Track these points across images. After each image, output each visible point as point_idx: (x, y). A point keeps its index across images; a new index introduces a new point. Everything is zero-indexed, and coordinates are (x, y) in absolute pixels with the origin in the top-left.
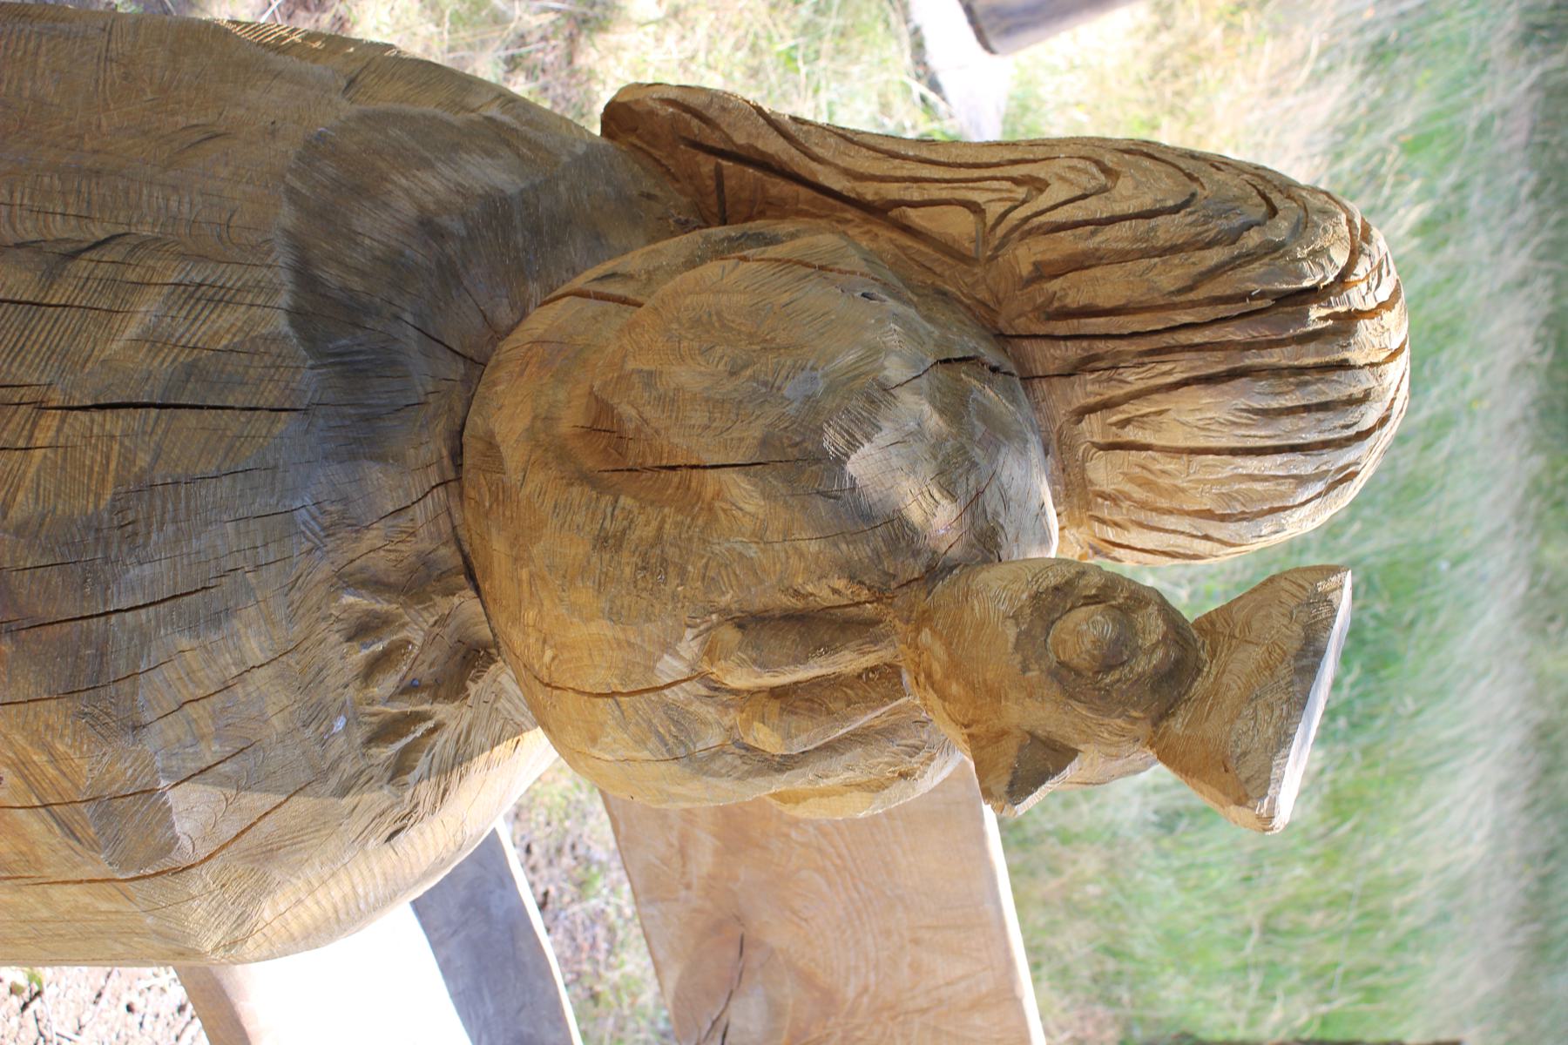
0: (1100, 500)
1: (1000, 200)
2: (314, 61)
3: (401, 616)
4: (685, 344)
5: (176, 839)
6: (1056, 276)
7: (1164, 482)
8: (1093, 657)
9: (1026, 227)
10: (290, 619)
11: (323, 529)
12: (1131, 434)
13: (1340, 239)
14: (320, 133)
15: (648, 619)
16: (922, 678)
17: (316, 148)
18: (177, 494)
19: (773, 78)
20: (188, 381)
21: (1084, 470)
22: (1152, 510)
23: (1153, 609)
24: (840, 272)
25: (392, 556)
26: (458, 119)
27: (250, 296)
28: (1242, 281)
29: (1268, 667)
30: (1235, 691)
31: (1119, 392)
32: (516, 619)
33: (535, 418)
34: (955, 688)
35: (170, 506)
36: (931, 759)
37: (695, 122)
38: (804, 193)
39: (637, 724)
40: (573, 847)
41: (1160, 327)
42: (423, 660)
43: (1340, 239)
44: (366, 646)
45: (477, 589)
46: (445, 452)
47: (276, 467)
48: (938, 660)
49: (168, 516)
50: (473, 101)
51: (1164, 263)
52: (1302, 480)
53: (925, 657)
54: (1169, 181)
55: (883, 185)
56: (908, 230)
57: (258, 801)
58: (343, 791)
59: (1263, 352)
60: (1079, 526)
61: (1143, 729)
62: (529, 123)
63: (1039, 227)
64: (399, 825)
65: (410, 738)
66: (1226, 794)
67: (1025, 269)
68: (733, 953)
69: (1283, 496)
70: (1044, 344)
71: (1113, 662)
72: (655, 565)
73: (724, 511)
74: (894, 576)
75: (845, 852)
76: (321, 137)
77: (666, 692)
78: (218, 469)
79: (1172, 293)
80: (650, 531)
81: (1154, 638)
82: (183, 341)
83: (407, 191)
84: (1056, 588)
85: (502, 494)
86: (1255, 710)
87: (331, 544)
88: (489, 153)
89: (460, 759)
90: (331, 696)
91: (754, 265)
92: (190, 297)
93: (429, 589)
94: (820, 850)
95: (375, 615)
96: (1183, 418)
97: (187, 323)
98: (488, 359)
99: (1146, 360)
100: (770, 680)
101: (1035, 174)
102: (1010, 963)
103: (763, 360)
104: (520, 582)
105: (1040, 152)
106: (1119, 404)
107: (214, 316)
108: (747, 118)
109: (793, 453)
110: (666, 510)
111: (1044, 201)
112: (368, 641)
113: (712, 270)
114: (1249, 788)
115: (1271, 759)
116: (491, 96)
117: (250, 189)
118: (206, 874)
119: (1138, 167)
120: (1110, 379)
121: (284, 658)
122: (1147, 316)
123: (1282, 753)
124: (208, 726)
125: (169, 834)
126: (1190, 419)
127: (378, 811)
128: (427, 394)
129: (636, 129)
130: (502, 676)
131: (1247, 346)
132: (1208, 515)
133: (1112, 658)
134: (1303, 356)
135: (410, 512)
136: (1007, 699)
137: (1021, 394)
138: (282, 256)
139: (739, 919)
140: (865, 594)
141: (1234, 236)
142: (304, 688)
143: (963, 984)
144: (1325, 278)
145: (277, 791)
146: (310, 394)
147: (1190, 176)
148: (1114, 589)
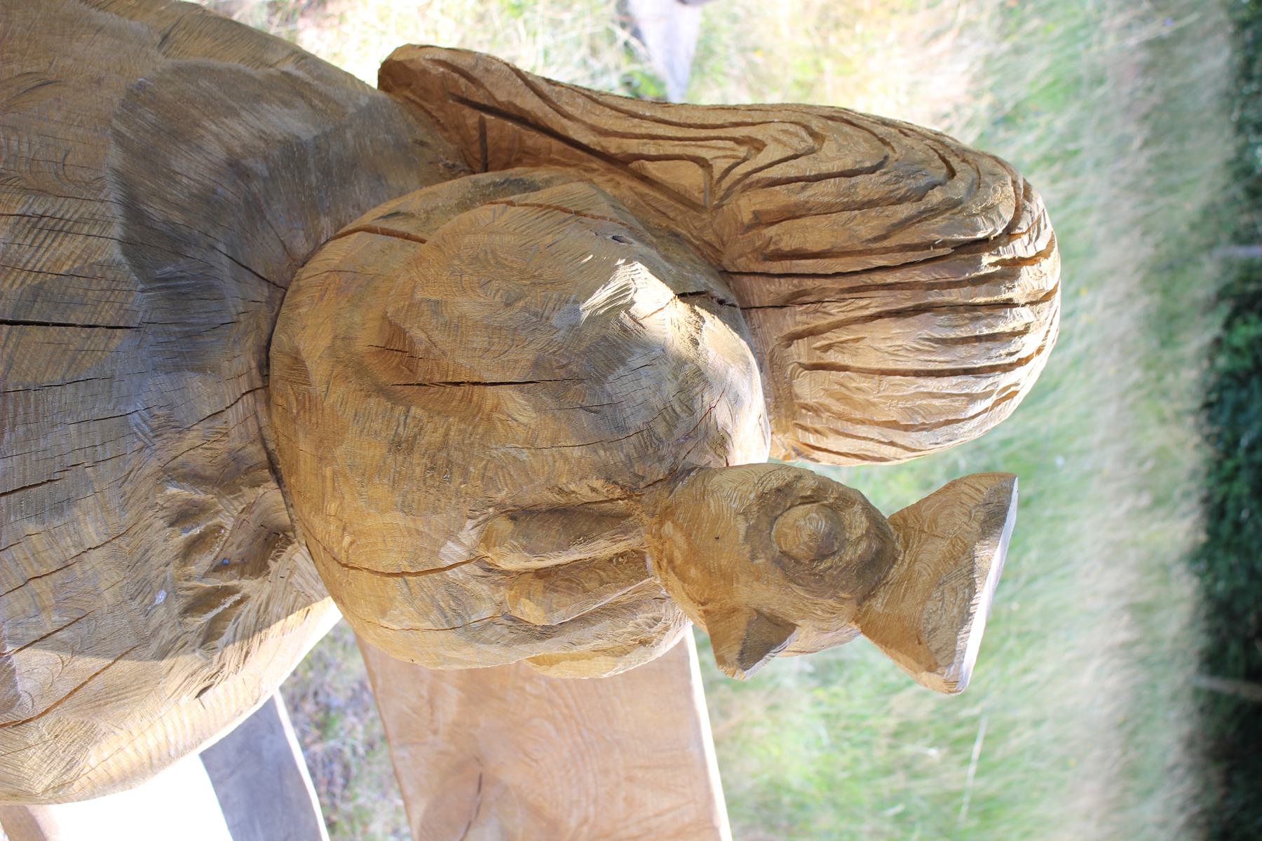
0: (804, 411)
1: (725, 157)
2: (131, 18)
3: (215, 505)
4: (466, 278)
5: (18, 696)
6: (772, 224)
7: (859, 397)
8: (810, 548)
9: (747, 181)
10: (123, 507)
11: (152, 431)
12: (832, 357)
13: (1007, 198)
14: (140, 83)
15: (435, 512)
16: (664, 563)
17: (137, 96)
18: (27, 399)
19: (498, 23)
20: (35, 301)
21: (791, 386)
22: (847, 420)
23: (857, 508)
24: (593, 217)
25: (208, 453)
26: (259, 73)
27: (86, 228)
28: (927, 232)
29: (953, 558)
30: (925, 578)
31: (822, 322)
32: (319, 509)
33: (335, 337)
34: (693, 572)
35: (21, 410)
36: (667, 629)
37: (462, 81)
38: (556, 144)
39: (422, 600)
40: (316, 694)
41: (859, 269)
42: (232, 543)
43: (1007, 198)
44: (186, 530)
45: (279, 481)
46: (253, 364)
47: (112, 377)
48: (679, 548)
49: (19, 419)
50: (272, 57)
51: (863, 215)
52: (972, 398)
53: (667, 545)
54: (867, 146)
55: (625, 141)
56: (645, 179)
57: (88, 664)
58: (162, 654)
59: (944, 292)
60: (785, 432)
61: (849, 608)
62: (320, 78)
63: (758, 182)
64: (207, 683)
65: (221, 609)
66: (919, 663)
67: (746, 217)
68: (472, 788)
69: (956, 411)
70: (761, 280)
71: (826, 553)
72: (441, 467)
73: (500, 420)
74: (643, 478)
75: (572, 703)
76: (141, 86)
77: (448, 572)
78: (63, 378)
79: (869, 241)
80: (437, 437)
81: (859, 532)
82: (30, 266)
83: (217, 136)
84: (778, 490)
85: (308, 403)
86: (943, 593)
87: (158, 443)
88: (286, 104)
89: (261, 625)
90: (154, 573)
91: (521, 209)
92: (34, 227)
93: (238, 481)
94: (550, 701)
95: (194, 504)
96: (876, 345)
97: (33, 250)
98: (289, 283)
99: (847, 296)
100: (536, 563)
101: (754, 135)
102: (710, 798)
103: (533, 294)
104: (324, 477)
105: (757, 117)
106: (823, 333)
107: (55, 244)
108: (507, 79)
109: (561, 373)
110: (451, 419)
111: (762, 159)
112: (188, 526)
113: (484, 213)
114: (938, 658)
115: (957, 634)
116: (286, 53)
117: (80, 131)
118: (43, 726)
119: (840, 132)
120: (817, 311)
121: (117, 541)
122: (848, 259)
123: (965, 629)
124: (49, 599)
125: (12, 692)
126: (882, 346)
127: (190, 671)
128: (238, 314)
129: (409, 85)
130: (297, 555)
131: (930, 286)
132: (894, 425)
133: (825, 549)
134: (977, 295)
135: (224, 415)
136: (738, 582)
137: (743, 324)
138: (113, 193)
139: (478, 760)
140: (618, 492)
141: (920, 194)
142: (132, 567)
143: (670, 816)
144: (995, 231)
145: (105, 654)
146: (141, 314)
147: (882, 141)
148: (826, 490)
